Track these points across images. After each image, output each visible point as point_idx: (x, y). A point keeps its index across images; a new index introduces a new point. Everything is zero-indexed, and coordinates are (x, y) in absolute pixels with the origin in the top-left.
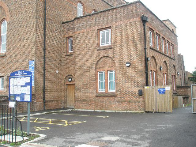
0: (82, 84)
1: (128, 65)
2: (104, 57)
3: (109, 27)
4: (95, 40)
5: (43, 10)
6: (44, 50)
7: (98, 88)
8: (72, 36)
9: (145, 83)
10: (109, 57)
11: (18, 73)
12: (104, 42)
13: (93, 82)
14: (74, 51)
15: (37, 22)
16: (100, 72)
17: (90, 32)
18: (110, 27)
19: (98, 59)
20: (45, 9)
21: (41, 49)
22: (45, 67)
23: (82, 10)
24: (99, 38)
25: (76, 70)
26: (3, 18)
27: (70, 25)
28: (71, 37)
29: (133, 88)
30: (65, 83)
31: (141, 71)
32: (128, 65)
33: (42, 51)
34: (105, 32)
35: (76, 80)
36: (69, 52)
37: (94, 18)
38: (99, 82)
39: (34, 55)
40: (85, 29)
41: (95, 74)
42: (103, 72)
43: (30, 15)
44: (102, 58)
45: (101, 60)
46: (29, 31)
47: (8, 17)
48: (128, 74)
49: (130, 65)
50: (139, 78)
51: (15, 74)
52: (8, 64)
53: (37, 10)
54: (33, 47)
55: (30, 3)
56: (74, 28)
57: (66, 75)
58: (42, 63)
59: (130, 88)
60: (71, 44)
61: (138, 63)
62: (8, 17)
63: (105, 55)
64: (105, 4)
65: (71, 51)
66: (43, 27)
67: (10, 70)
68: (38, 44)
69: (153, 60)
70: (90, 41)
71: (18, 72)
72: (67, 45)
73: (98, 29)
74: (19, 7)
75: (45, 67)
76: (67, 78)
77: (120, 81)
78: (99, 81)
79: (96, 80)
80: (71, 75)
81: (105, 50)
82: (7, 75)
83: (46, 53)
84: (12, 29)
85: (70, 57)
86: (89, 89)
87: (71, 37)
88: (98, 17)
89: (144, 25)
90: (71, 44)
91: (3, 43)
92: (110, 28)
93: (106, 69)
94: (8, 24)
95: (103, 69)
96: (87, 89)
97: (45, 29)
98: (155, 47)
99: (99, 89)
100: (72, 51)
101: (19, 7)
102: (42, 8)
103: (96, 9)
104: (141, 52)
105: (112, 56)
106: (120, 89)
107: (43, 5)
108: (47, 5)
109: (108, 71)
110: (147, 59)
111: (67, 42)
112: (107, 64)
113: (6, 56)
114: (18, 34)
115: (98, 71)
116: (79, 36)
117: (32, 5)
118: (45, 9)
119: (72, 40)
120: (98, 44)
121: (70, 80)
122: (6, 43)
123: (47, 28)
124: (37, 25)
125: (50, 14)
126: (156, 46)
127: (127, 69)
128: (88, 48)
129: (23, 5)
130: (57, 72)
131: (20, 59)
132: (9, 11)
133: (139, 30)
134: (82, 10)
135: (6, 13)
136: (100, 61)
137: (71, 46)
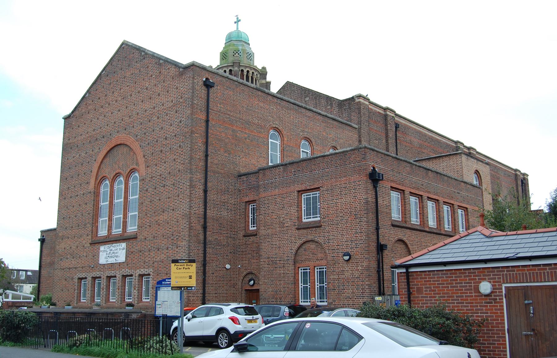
0: (271, 290)
1: (347, 258)
2: (309, 241)
3: (317, 189)
4: (293, 210)
5: (203, 158)
6: (205, 228)
7: (299, 298)
8: (255, 200)
9: (376, 289)
10: (317, 242)
11: (166, 282)
12: (308, 214)
13: (290, 286)
14: (258, 229)
15: (191, 181)
16: (302, 268)
17: (285, 196)
18: (319, 188)
19: (297, 245)
20: (207, 156)
21: (199, 228)
22: (205, 260)
23: (278, 143)
24: (302, 207)
25: (262, 263)
26: (131, 167)
27: (252, 179)
28: (254, 201)
29: (355, 299)
30: (242, 288)
31: (368, 268)
32: (347, 258)
33: (201, 232)
34: (311, 196)
35: (260, 283)
36: (251, 229)
37: (293, 171)
38: (300, 287)
39: (187, 239)
40: (277, 191)
41: (293, 272)
42: (308, 268)
43: (181, 167)
44: (304, 243)
45: (304, 247)
46: (178, 196)
47: (142, 168)
48: (347, 274)
49: (350, 259)
50: (364, 281)
51: (163, 283)
52: (141, 254)
53: (191, 159)
54: (184, 224)
55: (180, 146)
56: (258, 187)
57: (245, 273)
58: (201, 252)
59: (351, 299)
60: (254, 215)
61: (363, 254)
62: (142, 168)
63: (310, 237)
64: (331, 121)
65: (254, 227)
66: (202, 187)
67: (144, 264)
68: (193, 219)
69: (403, 246)
70: (285, 212)
71: (167, 280)
72: (246, 216)
73: (299, 191)
74: (161, 151)
75: (205, 260)
76: (247, 279)
77: (334, 286)
78: (300, 284)
79: (296, 283)
80: (252, 274)
81: (311, 229)
82: (137, 274)
83: (208, 233)
84: (149, 190)
85: (252, 239)
86: (283, 299)
87: (254, 201)
88: (299, 169)
89: (375, 187)
90: (254, 215)
91: (130, 214)
92: (318, 190)
93: (312, 264)
94: (142, 180)
95: (307, 263)
96: (280, 299)
97: (205, 191)
98: (406, 222)
99: (300, 300)
100: (255, 228)
101: (161, 151)
102: (200, 155)
103: (308, 136)
104: (367, 236)
105: (321, 240)
106: (335, 301)
107: (203, 148)
108: (210, 148)
109: (315, 267)
110: (381, 248)
111: (246, 209)
112: (313, 254)
113: (137, 238)
114: (160, 200)
115: (299, 268)
116: (266, 202)
117: (184, 151)
118: (207, 156)
119: (255, 207)
120: (300, 218)
121: (252, 282)
122: (137, 213)
123: (209, 189)
124: (191, 186)
125: (216, 162)
126: (407, 219)
127: (345, 265)
128: (282, 225)
129: (167, 149)
130: (228, 266)
131: (163, 245)
132: (144, 156)
133: (364, 197)
134: (278, 143)
135: (137, 160)
136: (302, 250)
137: (254, 217)
